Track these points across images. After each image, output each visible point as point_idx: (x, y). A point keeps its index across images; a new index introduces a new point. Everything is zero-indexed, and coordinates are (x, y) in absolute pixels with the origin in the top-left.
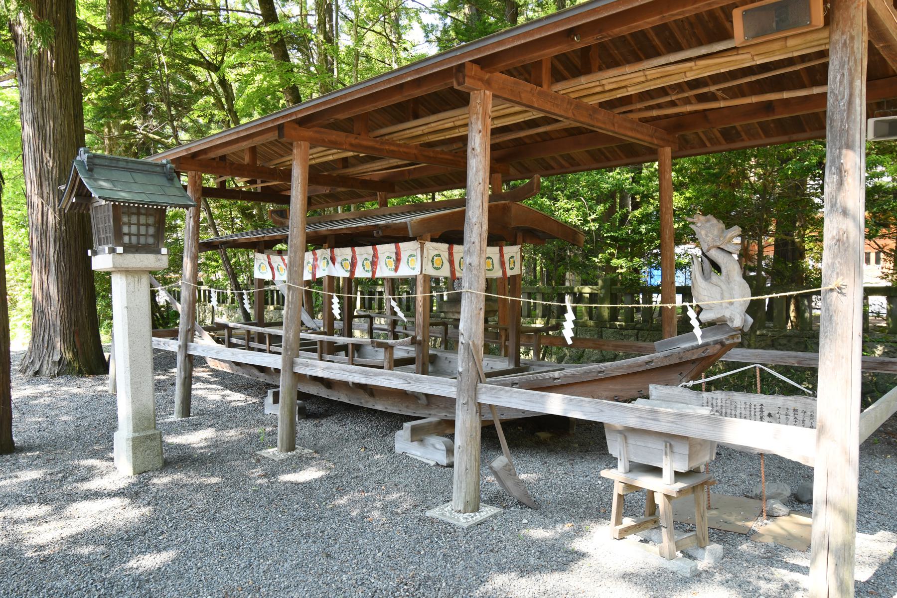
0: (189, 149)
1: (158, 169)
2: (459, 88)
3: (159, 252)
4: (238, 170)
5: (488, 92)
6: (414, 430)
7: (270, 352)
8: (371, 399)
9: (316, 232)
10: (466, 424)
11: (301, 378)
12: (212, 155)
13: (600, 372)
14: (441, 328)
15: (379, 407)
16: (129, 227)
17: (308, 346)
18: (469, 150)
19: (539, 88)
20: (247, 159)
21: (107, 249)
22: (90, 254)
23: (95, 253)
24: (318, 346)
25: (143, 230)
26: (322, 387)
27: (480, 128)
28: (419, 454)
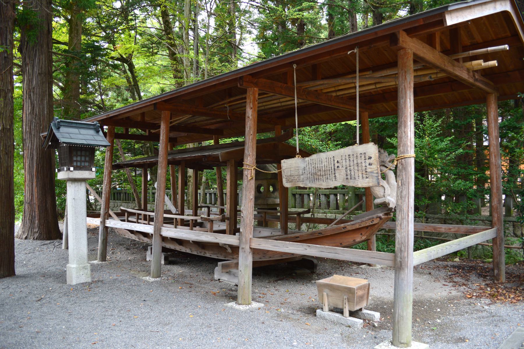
0: (108, 115)
1: (92, 127)
2: (241, 87)
3: (91, 170)
4: (136, 125)
5: (256, 89)
6: (223, 266)
7: (129, 221)
8: (203, 251)
9: (174, 159)
10: (246, 262)
11: (164, 239)
12: (121, 117)
13: (319, 233)
14: (206, 209)
15: (208, 255)
16: (81, 152)
17: (168, 221)
18: (246, 118)
19: (285, 85)
20: (139, 119)
21: (65, 168)
22: (57, 171)
23: (59, 171)
24: (174, 221)
25: (83, 159)
26: (177, 244)
27: (252, 106)
28: (226, 279)
